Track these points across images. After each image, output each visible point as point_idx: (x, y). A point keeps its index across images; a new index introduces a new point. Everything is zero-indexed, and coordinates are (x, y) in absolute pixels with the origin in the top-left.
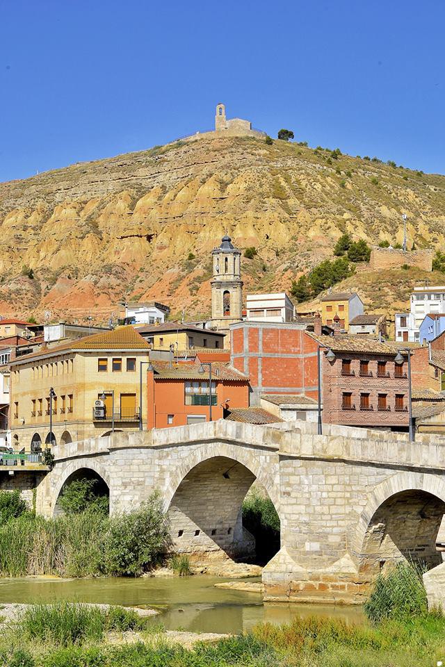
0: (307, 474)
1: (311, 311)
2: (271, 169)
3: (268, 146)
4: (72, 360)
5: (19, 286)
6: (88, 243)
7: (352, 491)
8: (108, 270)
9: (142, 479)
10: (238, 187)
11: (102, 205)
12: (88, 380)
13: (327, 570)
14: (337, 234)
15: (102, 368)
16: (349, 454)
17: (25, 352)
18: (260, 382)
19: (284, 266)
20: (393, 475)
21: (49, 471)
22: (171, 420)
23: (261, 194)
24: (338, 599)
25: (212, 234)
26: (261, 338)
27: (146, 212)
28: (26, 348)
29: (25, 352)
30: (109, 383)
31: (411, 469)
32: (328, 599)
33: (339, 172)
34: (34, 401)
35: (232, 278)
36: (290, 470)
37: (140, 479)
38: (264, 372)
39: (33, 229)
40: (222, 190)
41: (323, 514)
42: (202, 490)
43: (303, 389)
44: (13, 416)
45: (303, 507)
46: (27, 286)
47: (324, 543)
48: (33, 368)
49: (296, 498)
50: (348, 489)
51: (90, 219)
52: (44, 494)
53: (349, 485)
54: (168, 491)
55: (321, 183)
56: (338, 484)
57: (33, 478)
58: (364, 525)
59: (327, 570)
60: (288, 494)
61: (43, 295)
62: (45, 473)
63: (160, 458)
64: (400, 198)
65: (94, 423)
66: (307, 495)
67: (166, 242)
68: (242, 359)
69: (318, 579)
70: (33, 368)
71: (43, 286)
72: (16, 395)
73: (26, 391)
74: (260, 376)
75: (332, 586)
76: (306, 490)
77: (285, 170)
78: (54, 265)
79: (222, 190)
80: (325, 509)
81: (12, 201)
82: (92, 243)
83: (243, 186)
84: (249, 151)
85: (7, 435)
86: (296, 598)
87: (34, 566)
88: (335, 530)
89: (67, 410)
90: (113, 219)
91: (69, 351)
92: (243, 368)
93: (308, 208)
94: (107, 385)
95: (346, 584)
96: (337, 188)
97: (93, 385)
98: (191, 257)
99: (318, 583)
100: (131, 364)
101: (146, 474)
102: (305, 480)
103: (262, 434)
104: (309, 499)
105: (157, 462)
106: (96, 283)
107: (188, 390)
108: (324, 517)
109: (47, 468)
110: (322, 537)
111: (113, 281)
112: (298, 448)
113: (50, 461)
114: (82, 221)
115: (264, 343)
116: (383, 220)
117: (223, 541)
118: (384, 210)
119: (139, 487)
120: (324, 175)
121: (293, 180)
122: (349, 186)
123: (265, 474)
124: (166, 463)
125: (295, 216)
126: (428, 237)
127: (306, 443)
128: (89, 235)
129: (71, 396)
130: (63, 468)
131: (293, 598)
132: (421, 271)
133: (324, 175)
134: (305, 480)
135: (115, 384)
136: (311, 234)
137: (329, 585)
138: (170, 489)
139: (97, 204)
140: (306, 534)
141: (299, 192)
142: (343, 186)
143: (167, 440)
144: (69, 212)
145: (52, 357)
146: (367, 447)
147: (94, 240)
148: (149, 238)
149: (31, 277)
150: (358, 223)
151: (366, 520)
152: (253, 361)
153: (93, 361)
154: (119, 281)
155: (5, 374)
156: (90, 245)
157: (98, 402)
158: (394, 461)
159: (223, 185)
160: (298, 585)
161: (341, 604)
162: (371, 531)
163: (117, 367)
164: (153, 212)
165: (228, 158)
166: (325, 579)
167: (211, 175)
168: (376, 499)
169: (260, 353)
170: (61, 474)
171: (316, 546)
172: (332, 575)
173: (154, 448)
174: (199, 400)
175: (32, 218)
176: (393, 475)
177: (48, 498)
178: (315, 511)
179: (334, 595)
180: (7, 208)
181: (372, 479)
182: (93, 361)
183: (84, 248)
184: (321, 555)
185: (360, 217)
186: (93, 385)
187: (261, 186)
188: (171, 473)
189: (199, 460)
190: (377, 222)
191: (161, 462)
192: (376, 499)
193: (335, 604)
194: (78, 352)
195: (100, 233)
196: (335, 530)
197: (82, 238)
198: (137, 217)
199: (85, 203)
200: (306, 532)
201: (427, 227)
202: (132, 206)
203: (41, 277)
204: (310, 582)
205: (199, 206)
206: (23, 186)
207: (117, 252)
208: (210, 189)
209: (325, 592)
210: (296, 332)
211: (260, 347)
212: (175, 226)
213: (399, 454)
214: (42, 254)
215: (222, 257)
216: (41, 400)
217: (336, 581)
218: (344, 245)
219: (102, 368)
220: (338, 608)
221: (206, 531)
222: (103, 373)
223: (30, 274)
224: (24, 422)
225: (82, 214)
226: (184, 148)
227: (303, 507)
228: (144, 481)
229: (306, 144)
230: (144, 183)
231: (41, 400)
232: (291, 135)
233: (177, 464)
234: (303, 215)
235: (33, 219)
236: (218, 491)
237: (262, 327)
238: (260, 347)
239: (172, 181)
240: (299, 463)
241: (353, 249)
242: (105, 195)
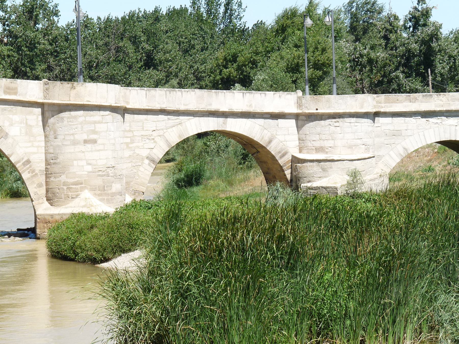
49: (104, 144)
50: (130, 134)
53: (130, 131)
58: (149, 164)
60: (94, 142)
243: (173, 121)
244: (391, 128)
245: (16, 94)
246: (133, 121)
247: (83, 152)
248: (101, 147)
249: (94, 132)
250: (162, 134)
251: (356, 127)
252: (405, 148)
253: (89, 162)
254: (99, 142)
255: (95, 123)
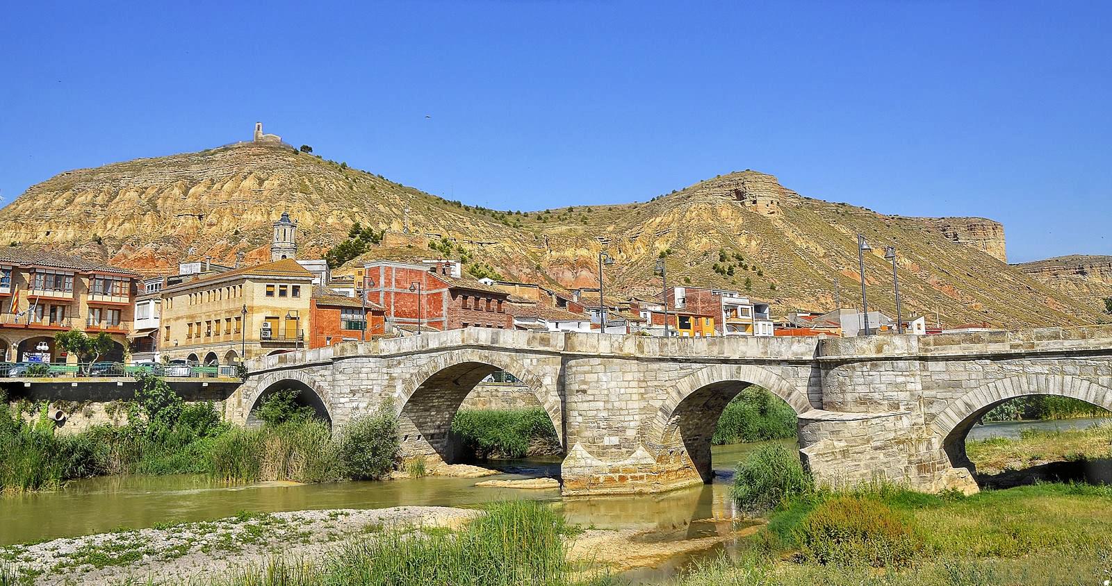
0: (605, 372)
1: (340, 276)
2: (298, 172)
3: (295, 155)
4: (241, 286)
5: (89, 250)
6: (148, 219)
7: (648, 386)
8: (167, 239)
9: (371, 387)
10: (272, 184)
11: (161, 190)
12: (256, 303)
13: (626, 462)
14: (349, 222)
15: (270, 294)
16: (643, 352)
17: (175, 282)
18: (392, 313)
19: (311, 243)
20: (701, 369)
21: (241, 384)
22: (328, 342)
23: (292, 190)
24: (637, 489)
25: (253, 217)
26: (394, 276)
27: (198, 197)
28: (177, 279)
29: (175, 282)
30: (275, 308)
31: (726, 361)
32: (627, 490)
33: (347, 178)
34: (190, 325)
35: (289, 245)
36: (587, 368)
37: (369, 387)
38: (396, 305)
39: (101, 206)
40: (261, 184)
41: (621, 409)
42: (431, 397)
43: (426, 320)
44: (163, 339)
45: (602, 404)
46: (96, 250)
47: (623, 437)
48: (190, 295)
49: (594, 395)
50: (644, 385)
51: (150, 201)
52: (235, 406)
53: (644, 381)
54: (401, 396)
55: (336, 185)
56: (633, 381)
57: (223, 391)
58: (663, 418)
59: (626, 462)
60: (584, 392)
61: (109, 258)
62: (237, 385)
63: (389, 367)
64: (390, 200)
65: (261, 343)
66: (606, 392)
67: (215, 221)
68: (378, 293)
69: (618, 471)
70: (190, 295)
71: (110, 251)
72: (168, 320)
73: (180, 316)
74: (393, 308)
75: (632, 477)
76: (605, 387)
77: (307, 174)
78: (119, 234)
79: (261, 184)
80: (623, 405)
81: (83, 184)
82: (152, 219)
83: (277, 183)
84: (281, 157)
85: (155, 357)
86: (596, 491)
87: (267, 471)
88: (632, 424)
89: (194, 336)
90: (169, 202)
91: (238, 277)
92: (378, 300)
93: (327, 202)
94: (274, 309)
95: (645, 474)
96: (347, 188)
97: (260, 309)
98: (237, 233)
99: (617, 475)
100: (296, 291)
101: (374, 382)
102: (604, 378)
103: (526, 338)
104: (607, 395)
105: (385, 370)
106: (156, 249)
107: (344, 316)
108: (622, 412)
109: (240, 380)
110: (620, 430)
111: (170, 248)
112: (595, 347)
113: (243, 373)
114: (144, 202)
115: (397, 281)
116: (381, 214)
117: (439, 445)
118: (381, 207)
119: (368, 394)
120: (338, 180)
121: (315, 181)
122: (355, 189)
123: (530, 377)
124: (396, 372)
125: (317, 207)
126: (412, 229)
127: (604, 342)
128: (149, 213)
129: (238, 319)
130: (259, 380)
131: (593, 492)
132: (421, 251)
133: (338, 180)
134: (604, 378)
135: (281, 308)
136: (330, 221)
137: (629, 477)
138: (403, 395)
139: (156, 190)
140: (605, 429)
141: (320, 190)
142: (351, 188)
143: (399, 349)
144: (132, 194)
145: (225, 282)
146: (666, 344)
147: (154, 217)
148: (200, 217)
149: (100, 243)
150: (364, 215)
151: (667, 413)
152: (388, 294)
153: (261, 288)
154: (175, 249)
155: (156, 301)
156: (150, 221)
157: (266, 324)
158: (703, 355)
159: (261, 182)
160: (598, 478)
161: (641, 494)
162: (669, 423)
163: (283, 293)
164: (204, 198)
165: (264, 162)
166: (625, 471)
167: (251, 173)
168: (679, 393)
169: (393, 288)
170: (257, 387)
171: (615, 440)
172: (631, 466)
173: (381, 357)
174: (353, 325)
175: (99, 198)
176: (701, 369)
177: (241, 409)
178: (613, 406)
179: (634, 486)
180: (78, 189)
181: (674, 375)
182: (261, 288)
183: (145, 223)
184: (621, 449)
185: (365, 210)
186: (260, 309)
187: (291, 183)
188: (404, 381)
189: (442, 366)
190: (377, 215)
191: (391, 370)
192: (679, 393)
193: (634, 494)
194: (248, 278)
195: (159, 212)
196: (632, 424)
197: (143, 215)
198: (189, 201)
199: (146, 188)
200: (605, 427)
201: (411, 222)
202: (186, 193)
203: (108, 243)
204: (609, 474)
205: (242, 195)
206: (93, 173)
207: (173, 227)
208: (250, 183)
209: (625, 483)
210: (421, 272)
211: (394, 283)
212: (222, 210)
213: (709, 349)
214: (109, 226)
215: (281, 229)
216: (199, 324)
217: (636, 472)
218: (356, 229)
219: (270, 294)
220: (637, 498)
221: (426, 436)
222: (270, 298)
223: (99, 241)
224: (177, 344)
225: (143, 196)
226: (230, 152)
227: (602, 404)
228: (372, 389)
229: (321, 157)
230: (195, 176)
231: (199, 324)
232: (310, 149)
233: (412, 371)
234: (323, 207)
235: (99, 200)
236: (443, 397)
237: (395, 266)
238: (394, 283)
239: (218, 176)
240: (598, 361)
241: (364, 233)
242: (163, 183)
243: (685, 371)
244: (946, 377)
245: (548, 345)
246: (647, 371)
247: (576, 402)
248: (591, 398)
249: (584, 382)
250: (674, 384)
251: (871, 377)
252: (967, 404)
253: (580, 413)
254: (589, 392)
255: (585, 373)
